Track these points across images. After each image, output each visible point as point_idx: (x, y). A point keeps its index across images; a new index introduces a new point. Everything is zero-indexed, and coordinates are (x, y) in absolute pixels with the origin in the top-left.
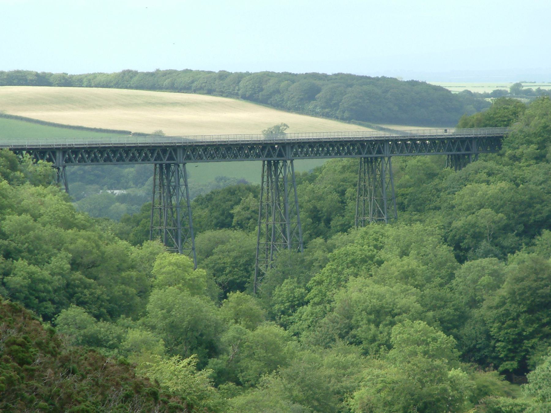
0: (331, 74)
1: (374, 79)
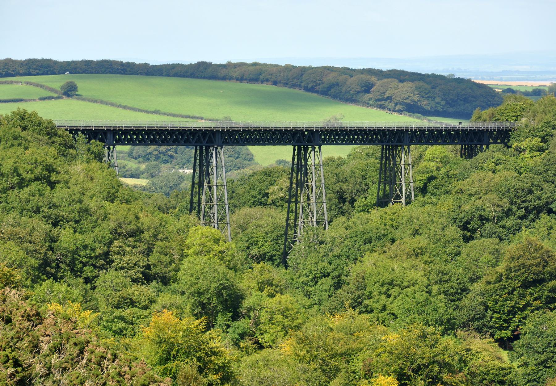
0: (386, 70)
1: (424, 75)
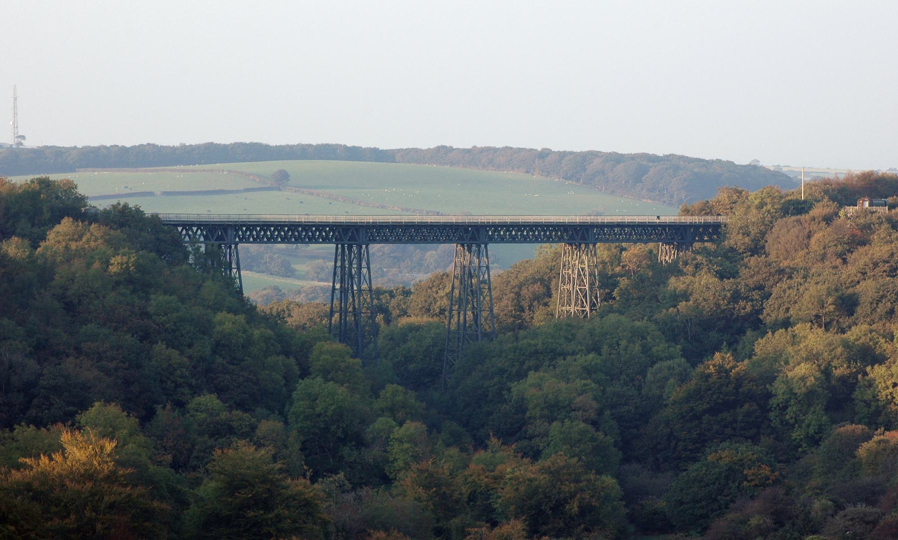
1: (707, 161)
